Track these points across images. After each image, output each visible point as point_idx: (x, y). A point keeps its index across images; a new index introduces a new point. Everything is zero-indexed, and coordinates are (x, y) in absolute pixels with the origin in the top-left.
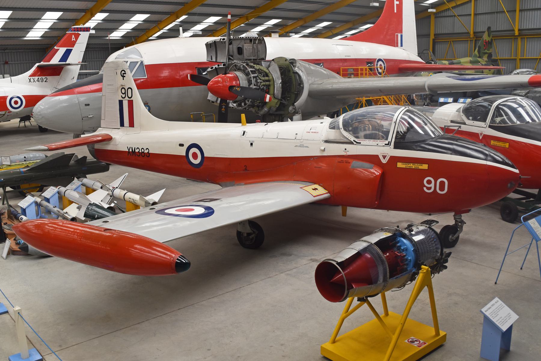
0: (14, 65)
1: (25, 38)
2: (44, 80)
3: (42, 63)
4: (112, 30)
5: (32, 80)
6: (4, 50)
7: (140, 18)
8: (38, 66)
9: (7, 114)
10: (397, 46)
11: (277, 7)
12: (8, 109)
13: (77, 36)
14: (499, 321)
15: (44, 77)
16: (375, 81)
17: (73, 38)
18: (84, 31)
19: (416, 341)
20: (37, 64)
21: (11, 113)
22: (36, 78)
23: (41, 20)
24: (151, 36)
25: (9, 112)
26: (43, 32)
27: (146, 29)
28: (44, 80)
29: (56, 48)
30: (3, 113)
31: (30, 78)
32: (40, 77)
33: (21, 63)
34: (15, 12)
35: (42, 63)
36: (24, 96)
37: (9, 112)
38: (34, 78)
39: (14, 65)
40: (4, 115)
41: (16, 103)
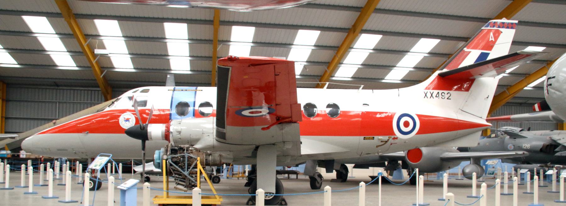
1: (383, 81)
2: (447, 96)
8: (440, 75)
9: (391, 140)
10: (202, 198)
13: (497, 34)
17: (491, 37)
18: (508, 28)
21: (396, 141)
24: (526, 86)
25: (394, 138)
26: (422, 57)
29: (465, 49)
30: (385, 138)
31: (426, 91)
32: (440, 92)
34: (385, 36)
36: (419, 116)
37: (394, 138)
38: (432, 91)
40: (386, 142)
41: (406, 124)
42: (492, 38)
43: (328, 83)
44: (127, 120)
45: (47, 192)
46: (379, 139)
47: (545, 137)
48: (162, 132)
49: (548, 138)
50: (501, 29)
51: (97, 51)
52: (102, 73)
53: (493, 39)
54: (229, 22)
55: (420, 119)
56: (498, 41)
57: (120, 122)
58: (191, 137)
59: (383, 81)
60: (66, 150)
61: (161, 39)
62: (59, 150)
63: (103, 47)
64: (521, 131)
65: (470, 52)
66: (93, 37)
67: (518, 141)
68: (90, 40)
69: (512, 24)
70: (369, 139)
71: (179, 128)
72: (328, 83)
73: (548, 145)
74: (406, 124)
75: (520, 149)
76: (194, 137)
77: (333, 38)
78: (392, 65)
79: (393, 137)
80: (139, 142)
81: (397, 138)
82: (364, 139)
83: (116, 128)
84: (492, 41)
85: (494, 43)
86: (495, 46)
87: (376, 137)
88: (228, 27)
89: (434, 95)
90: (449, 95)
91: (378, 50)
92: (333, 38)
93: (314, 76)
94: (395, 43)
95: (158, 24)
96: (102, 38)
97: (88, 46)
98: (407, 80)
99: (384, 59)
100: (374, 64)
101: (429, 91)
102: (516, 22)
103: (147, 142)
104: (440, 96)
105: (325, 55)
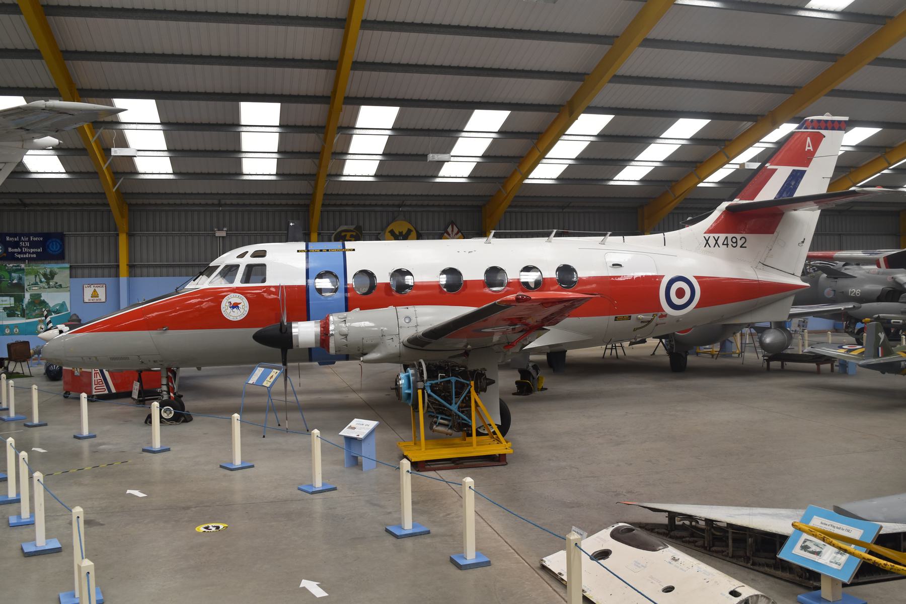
0: (93, 238)
1: (612, 183)
2: (740, 243)
3: (737, 201)
4: (622, 162)
5: (712, 242)
6: (563, 207)
7: (686, 129)
11: (886, 54)
12: (660, 309)
13: (817, 140)
14: (124, 302)
15: (738, 236)
16: (755, 515)
17: (809, 147)
18: (833, 129)
19: (65, 378)
20: (725, 205)
21: (665, 320)
22: (722, 236)
23: (659, 141)
25: (662, 316)
26: (676, 147)
27: (725, 140)
28: (740, 243)
31: (707, 236)
32: (730, 236)
33: (191, 235)
35: (737, 201)
37: (662, 316)
38: (716, 236)
39: (93, 238)
40: (649, 322)
41: (680, 293)
42: (809, 147)
43: (555, 231)
44: (235, 306)
45: (80, 428)
46: (638, 319)
47: (884, 276)
48: (316, 336)
49: (889, 278)
50: (822, 132)
51: (116, 152)
52: (114, 186)
53: (811, 148)
54: (356, 98)
55: (700, 283)
56: (817, 154)
57: (223, 310)
58: (365, 341)
59: (612, 183)
60: (128, 358)
61: (233, 126)
62: (112, 359)
63: (124, 144)
64: (844, 265)
65: (774, 171)
66: (109, 127)
67: (841, 282)
68: (101, 131)
69: (840, 122)
70: (623, 319)
71: (344, 328)
72: (555, 231)
73: (889, 291)
74: (680, 293)
75: (847, 298)
76: (368, 341)
77: (530, 120)
78: (628, 158)
79: (660, 314)
80: (279, 351)
81: (666, 316)
82: (616, 319)
83: (219, 321)
84: (809, 150)
85: (811, 154)
86: (814, 160)
87: (633, 316)
88: (351, 107)
89: (720, 242)
90: (743, 240)
91: (604, 136)
92: (311, 113)
93: (493, 178)
94: (634, 125)
95: (228, 104)
96: (123, 126)
97: (100, 141)
98: (651, 181)
99: (614, 150)
100: (598, 157)
101: (712, 235)
102: (846, 118)
103: (289, 351)
104: (730, 243)
105: (515, 146)
